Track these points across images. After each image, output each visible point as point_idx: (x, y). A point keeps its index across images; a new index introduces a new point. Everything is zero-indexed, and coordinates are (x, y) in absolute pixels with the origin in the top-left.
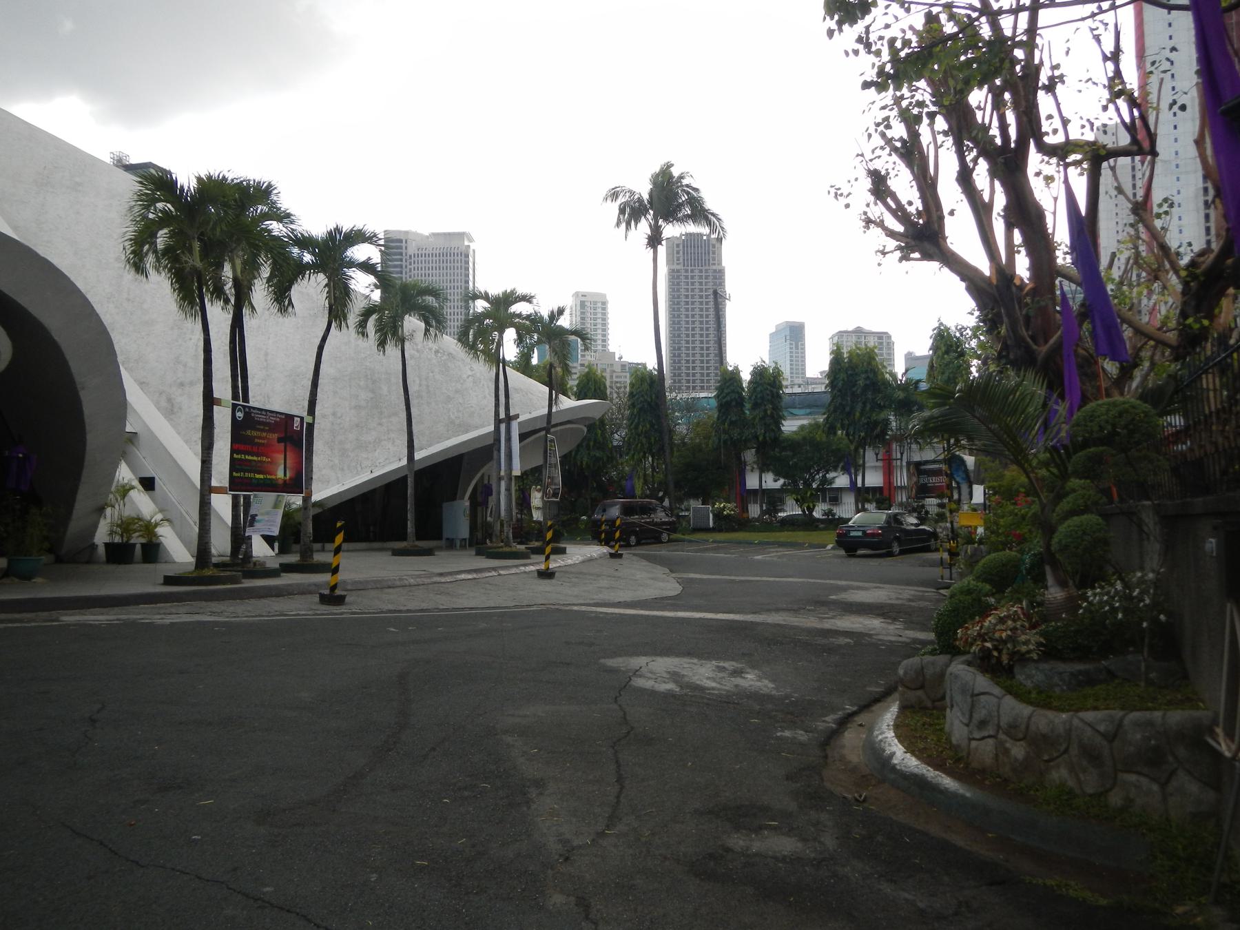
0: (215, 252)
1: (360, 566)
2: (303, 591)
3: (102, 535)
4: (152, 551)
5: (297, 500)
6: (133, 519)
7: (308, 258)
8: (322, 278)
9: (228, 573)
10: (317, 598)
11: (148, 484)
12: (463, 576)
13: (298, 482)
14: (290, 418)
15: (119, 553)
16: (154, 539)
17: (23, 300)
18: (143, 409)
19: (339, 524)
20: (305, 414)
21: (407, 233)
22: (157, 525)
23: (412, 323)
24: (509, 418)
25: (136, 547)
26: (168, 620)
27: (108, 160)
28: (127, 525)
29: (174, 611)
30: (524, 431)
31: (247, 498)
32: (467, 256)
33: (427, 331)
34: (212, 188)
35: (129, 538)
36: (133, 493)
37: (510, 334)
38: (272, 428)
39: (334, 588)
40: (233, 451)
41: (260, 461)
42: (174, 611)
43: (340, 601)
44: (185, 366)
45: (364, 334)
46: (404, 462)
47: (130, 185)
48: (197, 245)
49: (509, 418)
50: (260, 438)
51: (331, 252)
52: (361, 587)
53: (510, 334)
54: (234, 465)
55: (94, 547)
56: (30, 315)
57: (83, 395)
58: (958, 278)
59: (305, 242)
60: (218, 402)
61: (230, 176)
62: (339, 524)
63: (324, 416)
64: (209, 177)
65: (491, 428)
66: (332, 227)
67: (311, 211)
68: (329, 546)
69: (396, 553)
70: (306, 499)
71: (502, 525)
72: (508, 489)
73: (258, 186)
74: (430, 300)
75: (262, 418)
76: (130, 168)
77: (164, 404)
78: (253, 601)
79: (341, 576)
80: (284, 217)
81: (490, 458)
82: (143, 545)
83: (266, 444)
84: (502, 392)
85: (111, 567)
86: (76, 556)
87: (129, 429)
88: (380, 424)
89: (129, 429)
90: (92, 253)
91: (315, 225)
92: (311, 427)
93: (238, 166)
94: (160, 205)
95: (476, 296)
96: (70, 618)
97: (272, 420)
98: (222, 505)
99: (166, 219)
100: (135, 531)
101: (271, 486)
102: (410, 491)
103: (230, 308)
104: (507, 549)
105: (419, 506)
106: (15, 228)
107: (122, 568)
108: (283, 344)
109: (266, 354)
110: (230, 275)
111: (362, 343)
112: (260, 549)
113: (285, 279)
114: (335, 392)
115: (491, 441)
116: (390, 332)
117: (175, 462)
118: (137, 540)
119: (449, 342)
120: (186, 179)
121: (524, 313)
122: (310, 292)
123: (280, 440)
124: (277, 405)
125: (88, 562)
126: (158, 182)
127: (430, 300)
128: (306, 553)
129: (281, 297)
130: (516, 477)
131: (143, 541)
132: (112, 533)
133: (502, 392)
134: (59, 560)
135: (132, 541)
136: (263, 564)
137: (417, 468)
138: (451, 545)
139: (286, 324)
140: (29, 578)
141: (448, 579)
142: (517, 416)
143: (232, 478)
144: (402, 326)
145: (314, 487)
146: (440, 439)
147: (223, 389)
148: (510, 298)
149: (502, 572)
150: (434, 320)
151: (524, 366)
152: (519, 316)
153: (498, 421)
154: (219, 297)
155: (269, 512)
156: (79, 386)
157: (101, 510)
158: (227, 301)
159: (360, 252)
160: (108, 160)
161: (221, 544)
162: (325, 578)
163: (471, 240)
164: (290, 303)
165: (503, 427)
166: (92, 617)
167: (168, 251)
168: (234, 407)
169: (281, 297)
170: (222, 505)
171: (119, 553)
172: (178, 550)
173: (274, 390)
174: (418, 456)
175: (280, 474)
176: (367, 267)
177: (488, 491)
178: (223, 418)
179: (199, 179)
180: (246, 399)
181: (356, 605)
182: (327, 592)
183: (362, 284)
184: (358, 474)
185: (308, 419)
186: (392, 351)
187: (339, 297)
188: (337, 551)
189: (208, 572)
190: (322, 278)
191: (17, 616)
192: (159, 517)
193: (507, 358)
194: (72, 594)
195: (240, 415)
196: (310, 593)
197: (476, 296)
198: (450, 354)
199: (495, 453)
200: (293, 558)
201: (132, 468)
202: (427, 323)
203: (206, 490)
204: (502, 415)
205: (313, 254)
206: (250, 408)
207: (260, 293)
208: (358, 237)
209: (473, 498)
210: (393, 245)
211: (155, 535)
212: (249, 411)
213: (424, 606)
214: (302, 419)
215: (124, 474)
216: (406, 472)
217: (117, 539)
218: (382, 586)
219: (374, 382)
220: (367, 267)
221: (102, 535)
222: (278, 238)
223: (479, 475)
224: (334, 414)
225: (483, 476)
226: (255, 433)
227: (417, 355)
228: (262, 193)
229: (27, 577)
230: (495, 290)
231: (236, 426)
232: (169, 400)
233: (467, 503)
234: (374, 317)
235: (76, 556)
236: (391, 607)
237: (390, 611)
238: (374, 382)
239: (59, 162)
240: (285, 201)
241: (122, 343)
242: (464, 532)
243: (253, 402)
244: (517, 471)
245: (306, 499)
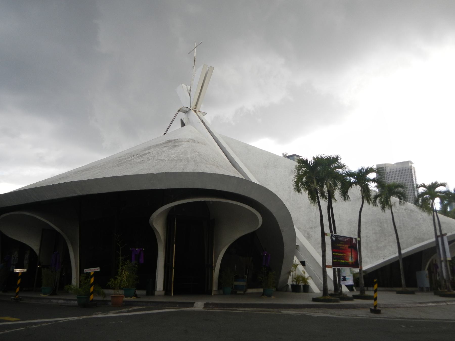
0: (321, 181)
1: (385, 298)
2: (363, 307)
3: (290, 282)
4: (306, 288)
5: (357, 270)
7: (353, 180)
8: (358, 187)
9: (334, 298)
10: (369, 310)
11: (303, 263)
12: (430, 304)
13: (357, 264)
14: (352, 239)
15: (296, 288)
17: (265, 205)
18: (301, 238)
19: (375, 280)
20: (356, 237)
21: (385, 164)
22: (307, 279)
23: (394, 199)
24: (442, 235)
25: (301, 287)
26: (316, 315)
27: (282, 155)
29: (317, 311)
30: (451, 240)
31: (339, 271)
32: (411, 170)
33: (400, 202)
34: (319, 161)
35: (299, 283)
37: (437, 200)
38: (346, 243)
39: (375, 306)
40: (333, 252)
41: (343, 256)
42: (317, 311)
43: (378, 312)
44: (312, 221)
45: (376, 205)
46: (397, 254)
47: (294, 164)
48: (315, 181)
49: (442, 235)
50: (342, 247)
51: (361, 177)
52: (386, 307)
53: (437, 200)
54: (334, 257)
55: (287, 286)
56: (266, 208)
59: (351, 174)
60: (326, 234)
61: (324, 156)
62: (375, 280)
63: (363, 237)
64: (317, 157)
65: (434, 239)
66: (360, 168)
67: (352, 164)
68: (371, 288)
69: (398, 292)
70: (361, 270)
71: (445, 281)
72: (446, 266)
73: (333, 158)
74: (401, 189)
75: (342, 239)
76: (289, 157)
77: (306, 235)
78: (344, 310)
79: (378, 301)
80: (343, 167)
81: (435, 252)
82: (303, 286)
83: (344, 249)
84: (437, 225)
85: (294, 294)
86: (282, 289)
87: (297, 244)
88: (385, 240)
89: (297, 244)
90: (282, 186)
91: (354, 167)
92: (359, 242)
93: (326, 152)
94: (303, 169)
95: (418, 187)
96: (284, 312)
97: (345, 240)
98: (330, 272)
99: (305, 173)
100: (300, 280)
101: (347, 265)
102: (401, 267)
103: (327, 200)
104: (449, 293)
105: (405, 272)
106: (259, 182)
107: (297, 294)
108: (347, 211)
109: (339, 215)
110: (326, 189)
111: (375, 208)
112: (345, 289)
113: (346, 188)
114: (366, 228)
115: (434, 245)
116: (386, 204)
117: (311, 255)
118: (301, 284)
119: (410, 205)
120: (310, 159)
121: (443, 191)
122: (355, 191)
123: (349, 247)
124: (345, 234)
126: (303, 162)
127: (401, 189)
128: (362, 291)
129: (344, 194)
130: (450, 261)
131: (303, 284)
132: (293, 281)
133: (437, 225)
134: (277, 290)
135: (300, 284)
136: (346, 295)
137: (403, 257)
138: (422, 290)
139: (346, 204)
141: (424, 305)
142: (445, 234)
143: (333, 262)
144: (390, 201)
145: (363, 264)
146: (411, 245)
147: (327, 230)
148: (435, 185)
149: (449, 303)
150: (403, 197)
151: (444, 211)
152: (440, 192)
153: (437, 237)
154: (323, 197)
155: (348, 273)
157: (289, 273)
158: (326, 198)
159: (372, 175)
160: (282, 155)
161: (331, 286)
162: (371, 302)
163: (412, 163)
164: (348, 197)
165: (440, 239)
166: (291, 312)
167: (306, 183)
168: (332, 235)
169: (344, 194)
170: (330, 272)
171: (296, 288)
172: (316, 289)
173: (345, 229)
174: (403, 252)
175: (350, 260)
176: (374, 180)
177: (436, 266)
178: (328, 240)
179: (314, 158)
180: (335, 232)
181: (386, 314)
182: (373, 308)
183: (372, 186)
184: (378, 259)
185: (358, 239)
186: (388, 211)
187: (366, 191)
188: (375, 291)
189: (328, 297)
190: (358, 187)
191: (268, 310)
193: (437, 209)
194: (16, 239)
195: (334, 238)
196: (366, 308)
197: (418, 187)
198: (411, 210)
199: (437, 250)
200: (358, 293)
202: (400, 199)
203: (325, 266)
204: (439, 234)
205: (355, 178)
206: (337, 236)
207: (337, 194)
208: (370, 170)
209: (429, 269)
210: (380, 170)
211: (307, 282)
212: (337, 237)
213: (415, 317)
214: (356, 239)
216: (398, 259)
217: (295, 283)
218: (395, 307)
219: (381, 223)
220: (374, 180)
221: (290, 282)
222: (341, 174)
223: (430, 260)
224: (367, 236)
225: (432, 260)
226: (340, 245)
227: (397, 211)
228: (335, 159)
229: (269, 296)
230: (428, 183)
231: (333, 243)
232: (308, 234)
233: (427, 272)
234: (378, 199)
235: (282, 289)
236: (400, 316)
237: (400, 318)
238: (381, 223)
239: (269, 159)
240: (343, 161)
241: (293, 215)
242: (427, 284)
243: (338, 234)
244: (449, 258)
245: (361, 270)
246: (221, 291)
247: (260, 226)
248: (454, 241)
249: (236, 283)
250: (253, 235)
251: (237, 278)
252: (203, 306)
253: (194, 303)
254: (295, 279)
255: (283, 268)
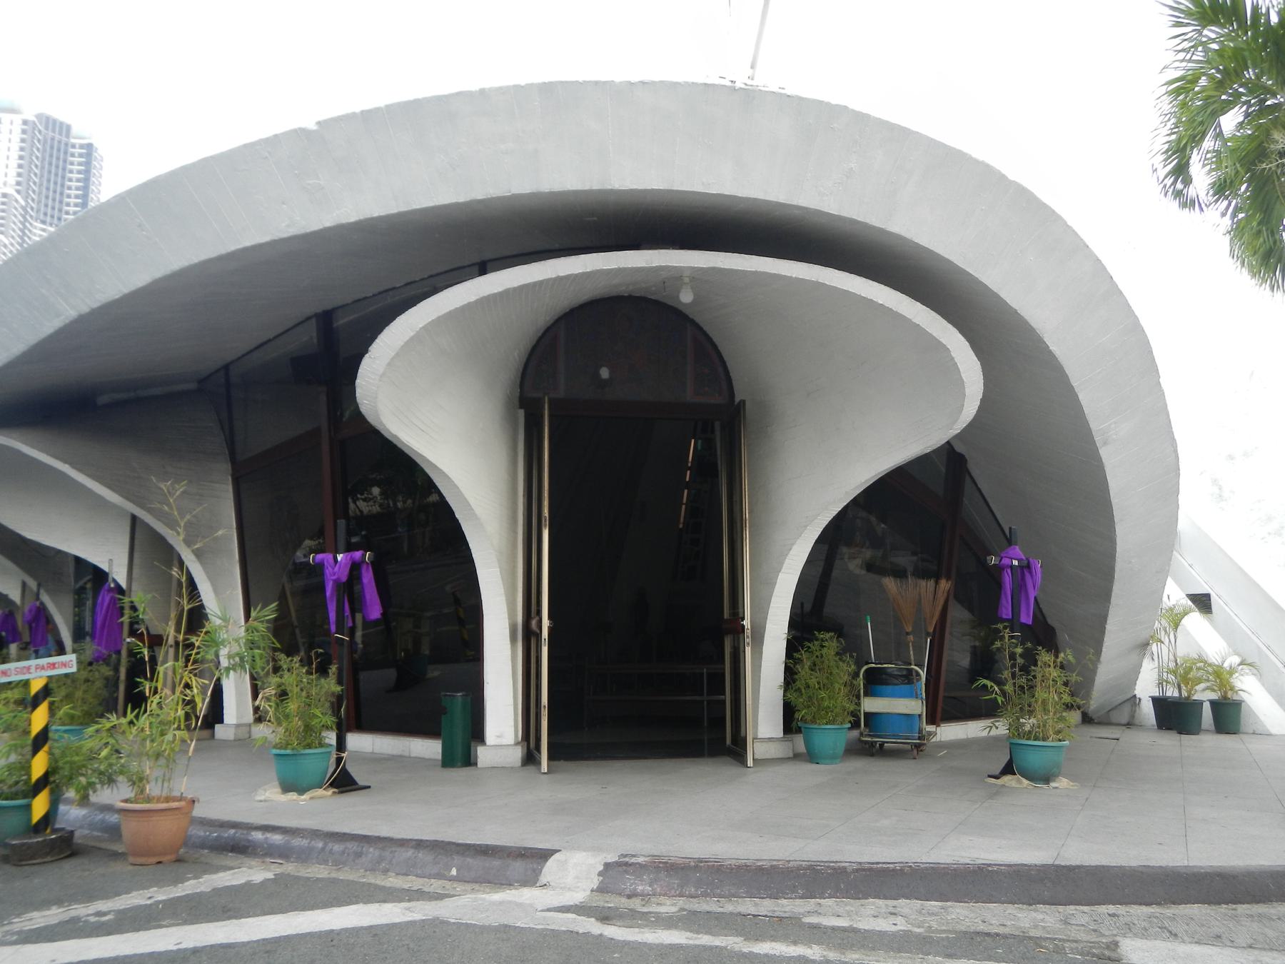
6: (1194, 662)
11: (1202, 602)
16: (1230, 694)
22: (1232, 671)
28: (1185, 672)
36: (1186, 621)
55: (1134, 701)
57: (1104, 453)
58: (851, 107)
118: (1204, 695)
125: (1129, 725)
131: (1214, 696)
132: (1161, 683)
134: (1087, 719)
140: (1047, 780)
156: (1098, 439)
192: (1235, 660)
201: (1178, 582)
215: (1174, 595)
217: (1171, 692)
221: (1146, 687)
246: (799, 741)
247: (970, 409)
248: (5, 660)
249: (871, 705)
250: (949, 464)
251: (876, 681)
252: (595, 882)
253: (545, 855)
254: (1174, 672)
255: (1111, 626)
